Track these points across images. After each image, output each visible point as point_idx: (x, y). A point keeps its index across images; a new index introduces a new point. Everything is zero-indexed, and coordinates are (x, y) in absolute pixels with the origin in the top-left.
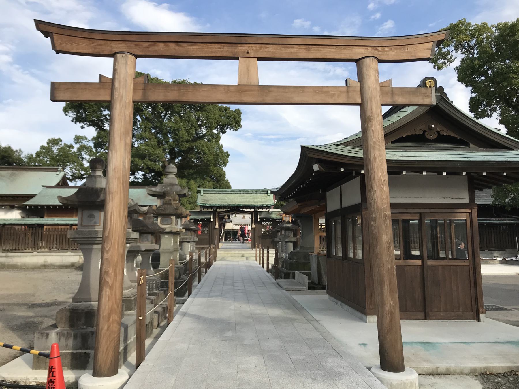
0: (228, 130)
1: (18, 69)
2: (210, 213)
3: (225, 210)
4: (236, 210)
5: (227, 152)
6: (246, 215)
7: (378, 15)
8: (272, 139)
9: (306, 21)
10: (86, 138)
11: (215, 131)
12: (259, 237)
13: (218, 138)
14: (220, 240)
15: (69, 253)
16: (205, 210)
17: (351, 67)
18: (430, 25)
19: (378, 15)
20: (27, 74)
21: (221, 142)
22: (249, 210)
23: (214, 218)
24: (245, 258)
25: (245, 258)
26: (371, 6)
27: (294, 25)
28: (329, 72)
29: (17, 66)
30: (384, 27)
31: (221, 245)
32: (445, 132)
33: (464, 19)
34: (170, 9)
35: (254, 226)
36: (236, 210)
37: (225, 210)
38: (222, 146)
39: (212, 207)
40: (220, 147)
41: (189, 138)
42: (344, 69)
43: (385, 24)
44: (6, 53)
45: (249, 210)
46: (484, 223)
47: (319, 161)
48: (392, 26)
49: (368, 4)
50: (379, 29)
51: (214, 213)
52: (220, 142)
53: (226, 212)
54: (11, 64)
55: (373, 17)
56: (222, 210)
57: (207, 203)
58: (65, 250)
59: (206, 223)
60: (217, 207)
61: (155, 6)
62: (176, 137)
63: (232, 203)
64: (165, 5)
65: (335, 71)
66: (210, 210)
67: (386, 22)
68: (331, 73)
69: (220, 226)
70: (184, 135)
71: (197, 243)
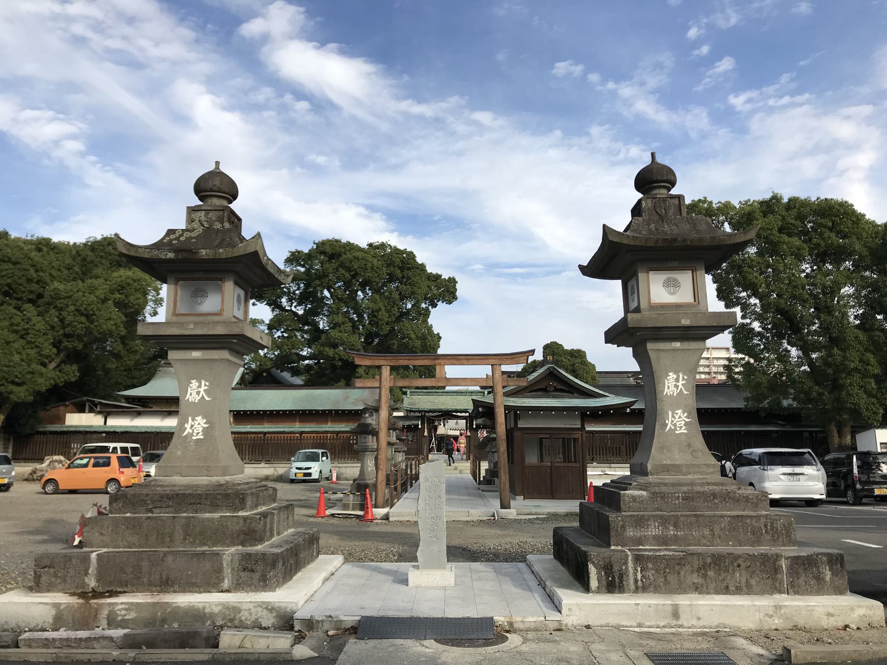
0: (440, 303)
1: (94, 164)
2: (417, 418)
3: (435, 414)
4: (448, 415)
5: (438, 334)
6: (459, 421)
7: (705, 50)
8: (517, 275)
9: (576, 64)
10: (263, 321)
11: (423, 306)
12: (475, 447)
13: (427, 313)
14: (430, 450)
15: (263, 465)
16: (412, 414)
17: (656, 144)
18: (802, 63)
19: (705, 50)
20: (109, 171)
21: (430, 321)
22: (463, 414)
23: (423, 424)
24: (457, 471)
25: (457, 471)
26: (693, 33)
27: (554, 71)
28: (618, 154)
29: (93, 158)
30: (715, 70)
31: (430, 456)
32: (559, 387)
33: (705, 198)
34: (342, 52)
35: (469, 434)
36: (448, 415)
37: (435, 414)
38: (431, 327)
39: (420, 412)
40: (430, 328)
41: (390, 320)
42: (643, 147)
43: (717, 64)
44: (74, 137)
45: (463, 414)
46: (740, 431)
47: (482, 406)
48: (731, 67)
49: (689, 28)
50: (708, 73)
51: (422, 418)
52: (429, 320)
53: (436, 416)
54: (82, 155)
55: (696, 52)
56: (431, 414)
57: (415, 407)
58: (258, 461)
59: (413, 429)
60: (426, 412)
61: (318, 48)
62: (375, 319)
63: (443, 407)
64: (333, 46)
65: (628, 151)
66: (417, 414)
67: (720, 60)
68: (621, 156)
69: (429, 432)
70: (384, 315)
71: (407, 453)
